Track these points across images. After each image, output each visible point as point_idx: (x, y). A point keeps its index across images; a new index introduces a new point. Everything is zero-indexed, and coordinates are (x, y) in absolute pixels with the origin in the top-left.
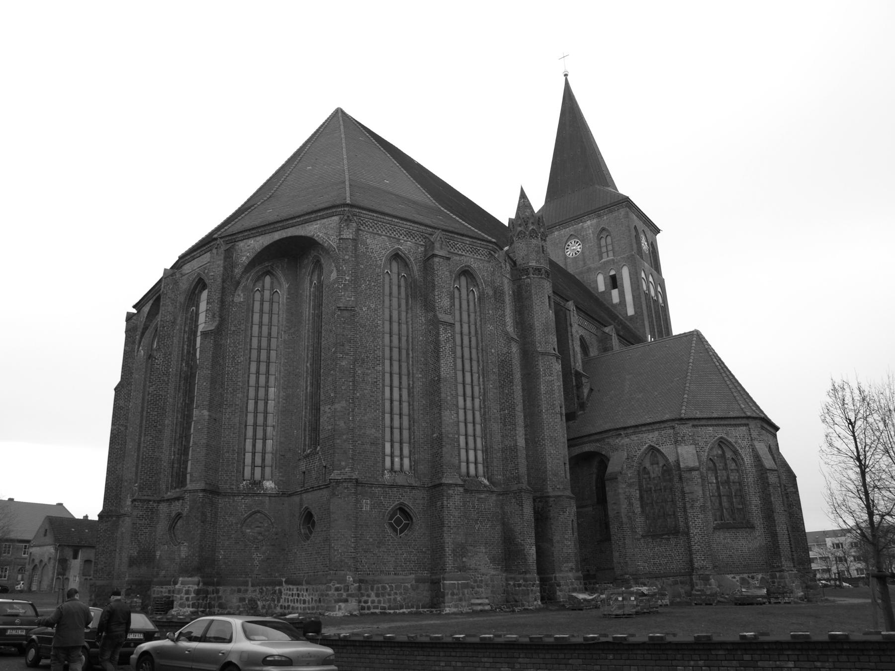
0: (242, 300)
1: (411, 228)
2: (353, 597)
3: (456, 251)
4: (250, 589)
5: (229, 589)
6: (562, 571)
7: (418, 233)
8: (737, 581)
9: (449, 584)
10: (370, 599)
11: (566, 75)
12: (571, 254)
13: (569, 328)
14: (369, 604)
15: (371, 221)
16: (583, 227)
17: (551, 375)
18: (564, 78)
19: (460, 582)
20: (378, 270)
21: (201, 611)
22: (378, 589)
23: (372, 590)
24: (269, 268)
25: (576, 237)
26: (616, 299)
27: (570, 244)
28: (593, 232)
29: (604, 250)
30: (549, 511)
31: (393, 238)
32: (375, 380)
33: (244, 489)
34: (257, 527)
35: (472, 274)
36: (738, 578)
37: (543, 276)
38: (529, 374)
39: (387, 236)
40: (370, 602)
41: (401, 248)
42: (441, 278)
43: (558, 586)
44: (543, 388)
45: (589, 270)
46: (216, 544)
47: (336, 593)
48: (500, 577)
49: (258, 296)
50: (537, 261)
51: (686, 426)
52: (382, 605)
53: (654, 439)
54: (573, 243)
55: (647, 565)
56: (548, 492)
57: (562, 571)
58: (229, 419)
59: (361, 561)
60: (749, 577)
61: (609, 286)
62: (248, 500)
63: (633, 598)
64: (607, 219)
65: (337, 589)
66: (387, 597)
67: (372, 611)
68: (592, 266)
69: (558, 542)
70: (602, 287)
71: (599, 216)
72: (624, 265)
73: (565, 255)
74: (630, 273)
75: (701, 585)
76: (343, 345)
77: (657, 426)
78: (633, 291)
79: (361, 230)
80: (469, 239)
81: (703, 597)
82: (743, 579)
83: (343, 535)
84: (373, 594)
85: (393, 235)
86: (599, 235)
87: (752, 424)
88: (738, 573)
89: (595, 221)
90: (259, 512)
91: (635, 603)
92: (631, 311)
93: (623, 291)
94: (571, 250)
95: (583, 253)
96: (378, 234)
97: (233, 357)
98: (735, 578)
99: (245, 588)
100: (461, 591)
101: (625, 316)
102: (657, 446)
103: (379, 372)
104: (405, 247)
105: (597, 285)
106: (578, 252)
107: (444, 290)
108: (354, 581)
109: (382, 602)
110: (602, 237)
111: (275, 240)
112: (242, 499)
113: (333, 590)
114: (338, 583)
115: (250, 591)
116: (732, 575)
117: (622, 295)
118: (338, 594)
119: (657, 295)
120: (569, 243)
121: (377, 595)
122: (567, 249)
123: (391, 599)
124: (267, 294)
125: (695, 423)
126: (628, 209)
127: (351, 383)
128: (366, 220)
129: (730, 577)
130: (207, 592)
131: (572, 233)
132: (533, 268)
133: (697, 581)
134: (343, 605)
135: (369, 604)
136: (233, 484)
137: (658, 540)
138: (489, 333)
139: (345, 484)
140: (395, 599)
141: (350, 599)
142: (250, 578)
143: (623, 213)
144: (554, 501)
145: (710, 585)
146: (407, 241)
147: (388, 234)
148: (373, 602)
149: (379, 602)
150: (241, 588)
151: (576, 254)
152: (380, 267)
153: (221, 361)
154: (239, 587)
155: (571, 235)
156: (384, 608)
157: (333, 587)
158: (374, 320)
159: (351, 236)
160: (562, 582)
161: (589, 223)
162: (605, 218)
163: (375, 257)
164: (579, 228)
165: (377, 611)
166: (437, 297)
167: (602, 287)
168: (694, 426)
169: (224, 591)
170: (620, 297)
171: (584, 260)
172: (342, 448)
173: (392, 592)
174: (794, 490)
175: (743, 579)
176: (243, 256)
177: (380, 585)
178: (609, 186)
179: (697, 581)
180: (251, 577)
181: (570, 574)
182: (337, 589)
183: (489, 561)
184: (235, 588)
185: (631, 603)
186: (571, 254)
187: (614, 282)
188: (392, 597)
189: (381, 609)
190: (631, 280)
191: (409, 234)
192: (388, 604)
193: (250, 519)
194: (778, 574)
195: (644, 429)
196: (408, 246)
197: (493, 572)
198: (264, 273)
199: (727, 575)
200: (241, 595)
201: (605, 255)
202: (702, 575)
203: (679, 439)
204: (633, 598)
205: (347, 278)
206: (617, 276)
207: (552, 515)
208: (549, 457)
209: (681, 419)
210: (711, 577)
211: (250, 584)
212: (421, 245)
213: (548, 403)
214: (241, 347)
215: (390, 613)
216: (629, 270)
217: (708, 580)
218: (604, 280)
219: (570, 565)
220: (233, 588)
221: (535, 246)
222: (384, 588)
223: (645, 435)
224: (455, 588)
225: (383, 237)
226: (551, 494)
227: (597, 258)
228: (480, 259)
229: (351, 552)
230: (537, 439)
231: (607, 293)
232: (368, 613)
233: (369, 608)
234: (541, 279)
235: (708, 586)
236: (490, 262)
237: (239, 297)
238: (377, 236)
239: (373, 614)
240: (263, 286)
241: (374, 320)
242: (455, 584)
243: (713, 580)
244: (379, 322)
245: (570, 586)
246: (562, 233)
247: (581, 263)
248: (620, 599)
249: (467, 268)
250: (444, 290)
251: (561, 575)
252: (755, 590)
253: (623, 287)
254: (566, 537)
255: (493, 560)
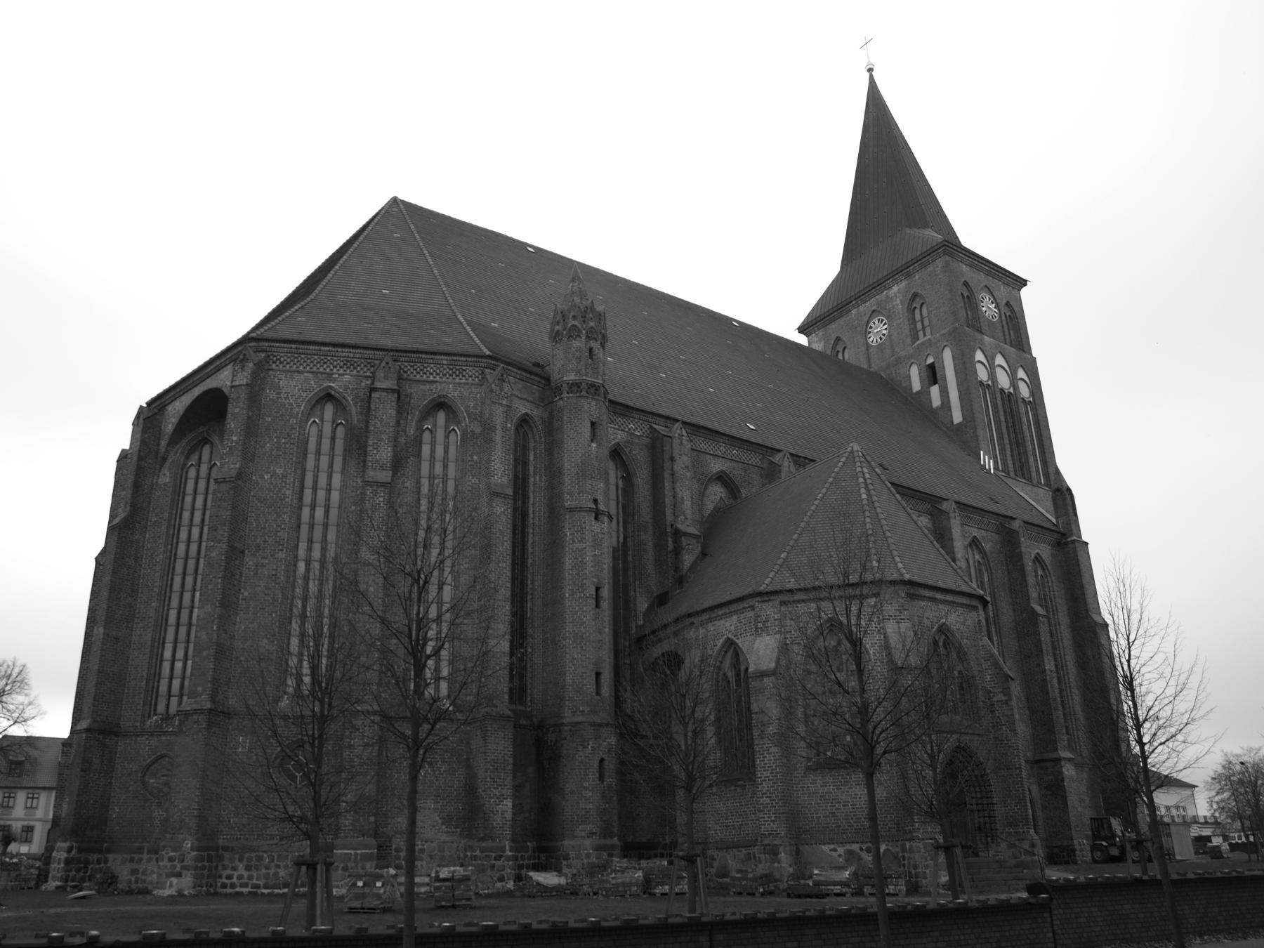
0: (168, 480)
1: (352, 355)
2: (188, 870)
3: (418, 376)
4: (145, 856)
5: (119, 857)
6: (576, 837)
7: (363, 361)
8: (840, 856)
9: (341, 854)
10: (236, 874)
11: (870, 70)
12: (875, 341)
13: (667, 465)
14: (234, 880)
15: (289, 355)
16: (888, 297)
17: (582, 540)
18: (868, 74)
19: (359, 852)
20: (293, 421)
21: (71, 887)
22: (249, 860)
23: (241, 860)
24: (205, 434)
25: (880, 313)
26: (936, 401)
27: (873, 326)
28: (901, 300)
29: (919, 326)
30: (562, 746)
31: (322, 373)
32: (274, 573)
33: (150, 726)
34: (164, 776)
35: (450, 407)
36: (841, 850)
37: (584, 393)
38: (554, 542)
39: (312, 372)
40: (235, 877)
41: (333, 385)
42: (381, 420)
43: (564, 859)
44: (568, 562)
45: (898, 361)
46: (109, 799)
47: (169, 864)
48: (456, 845)
49: (192, 473)
50: (579, 372)
51: (771, 604)
52: (255, 882)
53: (732, 628)
54: (877, 323)
55: (719, 828)
56: (564, 717)
57: (576, 837)
58: (140, 636)
59: (229, 821)
60: (861, 849)
61: (926, 381)
62: (154, 741)
63: (379, 884)
64: (919, 278)
65: (171, 859)
66: (264, 871)
67: (238, 889)
68: (903, 354)
69: (573, 792)
70: (916, 386)
71: (908, 276)
72: (945, 346)
73: (867, 343)
74: (953, 357)
75: (766, 862)
76: (215, 530)
77: (733, 607)
78: (959, 384)
79: (272, 370)
80: (446, 358)
81: (744, 883)
82: (850, 853)
83: (187, 785)
84: (241, 866)
85: (321, 370)
86: (910, 304)
87: (887, 592)
88: (842, 843)
89: (904, 284)
90: (165, 756)
91: (382, 891)
92: (957, 417)
93: (946, 387)
94: (874, 334)
95: (890, 336)
96: (299, 372)
97: (151, 556)
98: (835, 850)
99: (140, 856)
100: (359, 865)
101: (949, 425)
102: (734, 639)
103: (281, 561)
104: (340, 383)
105: (910, 382)
106: (884, 335)
107: (384, 437)
108: (192, 849)
109: (255, 878)
110: (915, 308)
111: (195, 397)
112: (147, 739)
113: (166, 860)
114: (173, 851)
115: (145, 861)
116: (832, 846)
117: (944, 393)
118: (171, 865)
119: (1014, 383)
120: (871, 324)
121: (248, 868)
122: (870, 333)
123: (269, 874)
124: (204, 468)
125: (787, 597)
126: (947, 258)
127: (220, 581)
128: (282, 354)
129: (826, 848)
130: (87, 862)
131: (874, 308)
132: (568, 384)
133: (761, 856)
134: (174, 880)
135: (234, 880)
136: (137, 721)
137: (733, 788)
138: (470, 488)
139: (195, 717)
140: (276, 875)
141: (184, 872)
142: (148, 842)
143: (940, 265)
144: (570, 730)
145: (779, 863)
146: (343, 375)
147: (315, 369)
148: (240, 877)
149: (250, 877)
150: (134, 855)
151: (881, 339)
152: (296, 417)
153: (132, 563)
154: (133, 855)
155: (874, 311)
156: (258, 887)
157: (166, 856)
158: (280, 491)
159: (245, 382)
160: (572, 854)
161: (895, 288)
162: (917, 277)
163: (291, 404)
164: (884, 298)
165: (245, 890)
166: (370, 448)
167: (916, 386)
168: (783, 603)
169: (115, 860)
170: (941, 396)
171: (892, 347)
172: (200, 669)
173: (272, 864)
174: (1004, 698)
175: (850, 853)
176: (169, 423)
177: (253, 855)
178: (926, 226)
179: (761, 856)
180: (149, 842)
181: (587, 842)
182: (171, 859)
183: (440, 821)
184: (127, 856)
185: (375, 891)
186: (875, 341)
187: (933, 374)
188: (272, 871)
189: (252, 888)
190: (955, 367)
191: (348, 364)
192: (264, 881)
193: (156, 765)
194: (907, 844)
195: (720, 613)
196: (343, 381)
197: (444, 837)
198: (200, 441)
199: (823, 847)
200: (134, 866)
201: (921, 334)
202: (769, 845)
203: (760, 625)
204: (379, 884)
205: (235, 438)
206: (936, 365)
207: (565, 752)
208: (571, 665)
209: (761, 594)
210: (781, 849)
211: (146, 850)
212: (367, 377)
213: (574, 582)
214: (161, 541)
215: (263, 894)
216: (952, 352)
217: (776, 854)
218: (919, 373)
219: (589, 827)
220: (125, 856)
221: (577, 351)
222: (260, 859)
223: (722, 622)
224: (350, 859)
225: (306, 374)
226: (566, 721)
227: (909, 340)
228: (465, 384)
229: (194, 809)
230: (557, 639)
231: (925, 392)
232: (231, 894)
233: (233, 886)
234: (579, 399)
235: (776, 864)
236: (482, 385)
237: (165, 477)
238: (296, 374)
239: (238, 894)
240: (200, 459)
241: (280, 491)
242: (351, 854)
243: (783, 854)
244: (287, 492)
245: (585, 861)
246: (862, 309)
247: (888, 351)
248: (360, 884)
249: (443, 400)
250: (384, 437)
251: (572, 843)
252: (833, 872)
253: (946, 381)
254: (586, 784)
255: (447, 820)
